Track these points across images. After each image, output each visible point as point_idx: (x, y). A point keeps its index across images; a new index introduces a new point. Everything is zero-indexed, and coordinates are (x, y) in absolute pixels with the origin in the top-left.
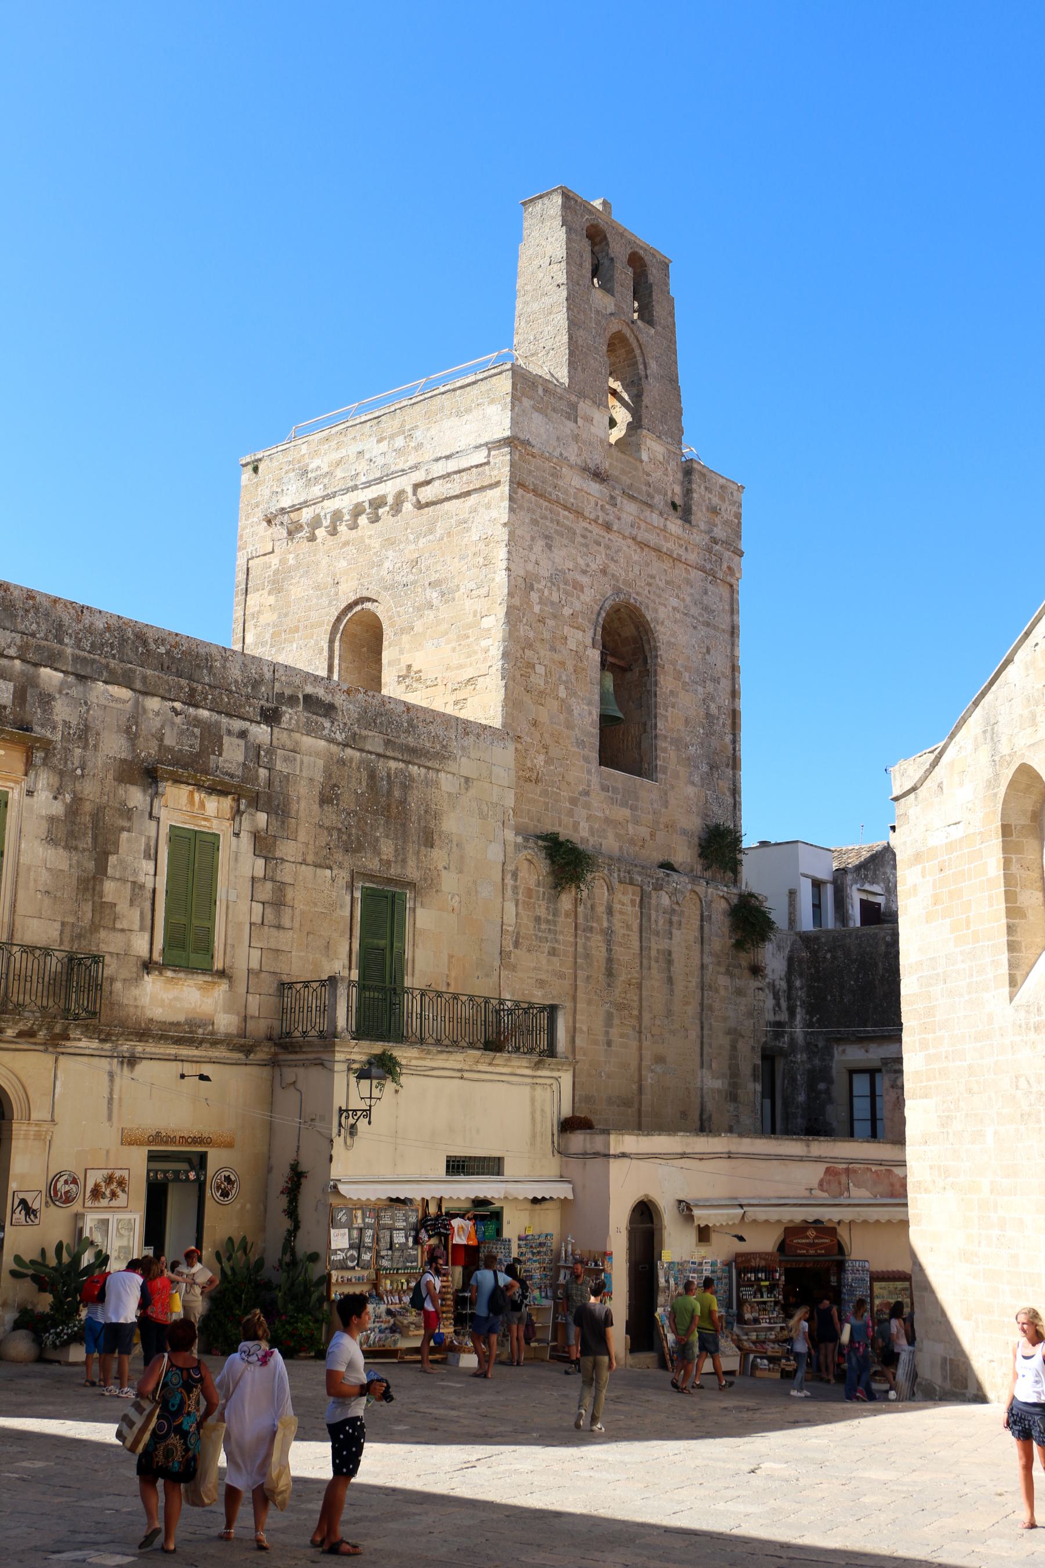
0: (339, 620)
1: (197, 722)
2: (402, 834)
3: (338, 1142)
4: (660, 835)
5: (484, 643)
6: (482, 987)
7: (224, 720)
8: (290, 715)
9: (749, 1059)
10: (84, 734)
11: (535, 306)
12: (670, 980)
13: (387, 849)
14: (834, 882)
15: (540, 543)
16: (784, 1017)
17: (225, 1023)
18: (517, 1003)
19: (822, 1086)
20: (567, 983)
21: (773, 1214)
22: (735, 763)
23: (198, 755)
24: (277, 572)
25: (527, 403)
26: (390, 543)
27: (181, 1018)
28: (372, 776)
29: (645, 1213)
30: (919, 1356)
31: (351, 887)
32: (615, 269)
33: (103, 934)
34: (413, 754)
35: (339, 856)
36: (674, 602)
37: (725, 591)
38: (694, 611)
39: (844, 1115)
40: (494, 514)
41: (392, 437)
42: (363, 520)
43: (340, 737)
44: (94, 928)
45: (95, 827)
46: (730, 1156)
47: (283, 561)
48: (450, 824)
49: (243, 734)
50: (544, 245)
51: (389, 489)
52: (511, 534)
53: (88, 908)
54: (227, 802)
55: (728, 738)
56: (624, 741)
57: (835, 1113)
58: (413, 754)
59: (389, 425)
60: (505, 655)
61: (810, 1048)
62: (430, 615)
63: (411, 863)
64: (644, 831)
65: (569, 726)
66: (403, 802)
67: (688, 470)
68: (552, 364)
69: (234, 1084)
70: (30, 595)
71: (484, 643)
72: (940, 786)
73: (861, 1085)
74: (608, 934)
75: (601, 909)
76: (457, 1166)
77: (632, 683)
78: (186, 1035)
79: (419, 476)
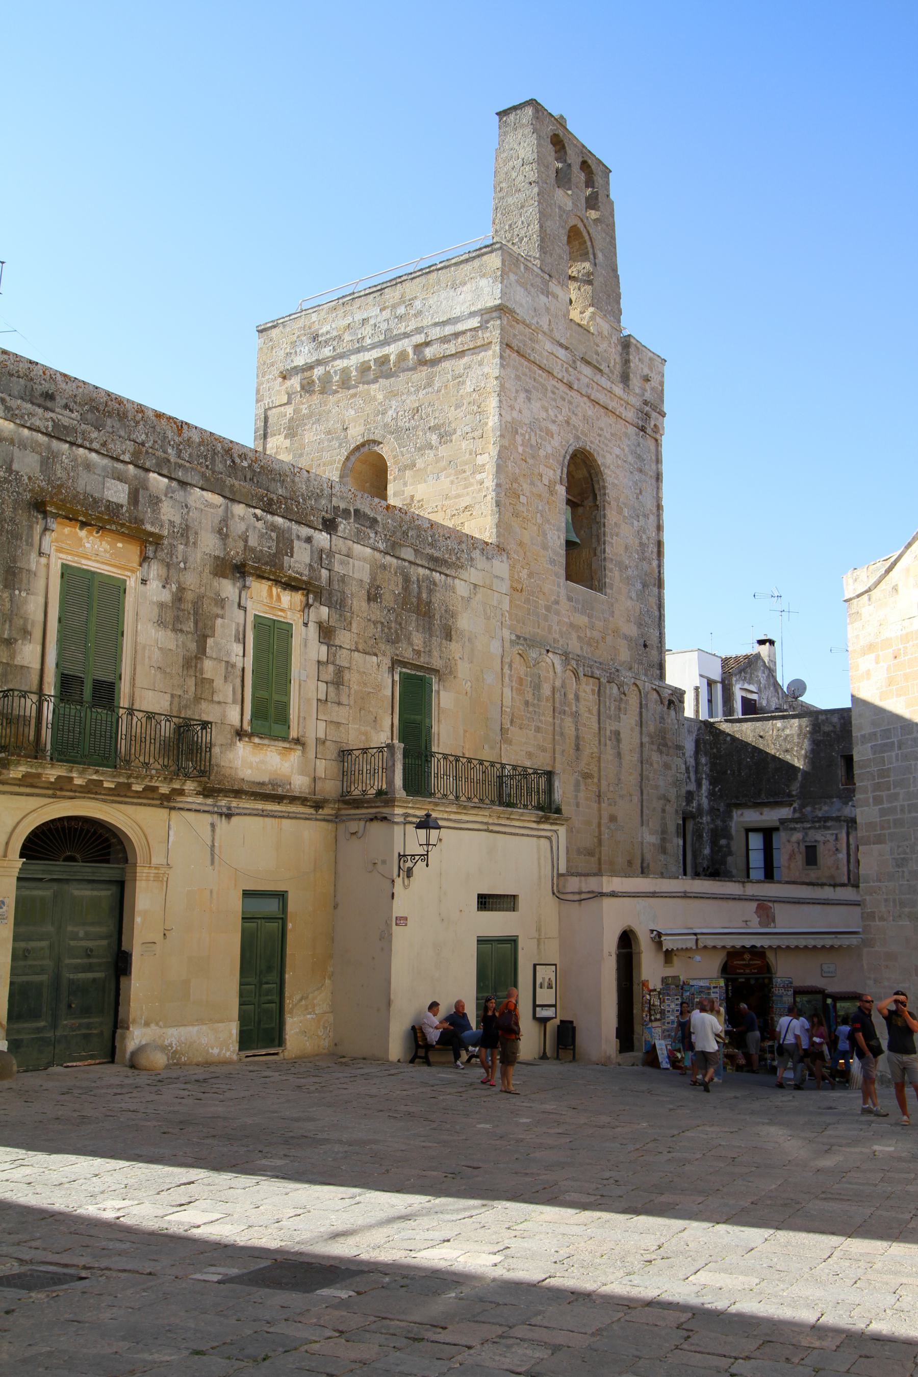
1: (274, 527)
2: (429, 630)
3: (399, 881)
4: (609, 639)
5: (479, 477)
6: (487, 754)
7: (295, 526)
8: (344, 526)
9: (673, 821)
10: (185, 532)
12: (619, 755)
15: (522, 395)
16: (692, 787)
17: (299, 783)
19: (723, 842)
22: (660, 584)
23: (275, 555)
25: (513, 277)
27: (265, 779)
28: (407, 580)
29: (627, 939)
31: (392, 669)
33: (204, 705)
34: (436, 563)
36: (617, 451)
37: (651, 444)
38: (630, 459)
40: (486, 370)
41: (394, 307)
43: (381, 546)
44: (198, 699)
45: (196, 613)
46: (685, 896)
48: (464, 622)
49: (309, 540)
53: (191, 682)
55: (655, 563)
56: (583, 560)
57: (734, 862)
58: (436, 563)
61: (713, 811)
62: (430, 454)
63: (436, 653)
64: (596, 634)
65: (545, 547)
66: (429, 603)
67: (626, 344)
69: (307, 834)
70: (141, 409)
72: (895, 589)
73: (756, 841)
74: (576, 715)
75: (571, 696)
76: (486, 902)
78: (271, 795)
79: (419, 339)
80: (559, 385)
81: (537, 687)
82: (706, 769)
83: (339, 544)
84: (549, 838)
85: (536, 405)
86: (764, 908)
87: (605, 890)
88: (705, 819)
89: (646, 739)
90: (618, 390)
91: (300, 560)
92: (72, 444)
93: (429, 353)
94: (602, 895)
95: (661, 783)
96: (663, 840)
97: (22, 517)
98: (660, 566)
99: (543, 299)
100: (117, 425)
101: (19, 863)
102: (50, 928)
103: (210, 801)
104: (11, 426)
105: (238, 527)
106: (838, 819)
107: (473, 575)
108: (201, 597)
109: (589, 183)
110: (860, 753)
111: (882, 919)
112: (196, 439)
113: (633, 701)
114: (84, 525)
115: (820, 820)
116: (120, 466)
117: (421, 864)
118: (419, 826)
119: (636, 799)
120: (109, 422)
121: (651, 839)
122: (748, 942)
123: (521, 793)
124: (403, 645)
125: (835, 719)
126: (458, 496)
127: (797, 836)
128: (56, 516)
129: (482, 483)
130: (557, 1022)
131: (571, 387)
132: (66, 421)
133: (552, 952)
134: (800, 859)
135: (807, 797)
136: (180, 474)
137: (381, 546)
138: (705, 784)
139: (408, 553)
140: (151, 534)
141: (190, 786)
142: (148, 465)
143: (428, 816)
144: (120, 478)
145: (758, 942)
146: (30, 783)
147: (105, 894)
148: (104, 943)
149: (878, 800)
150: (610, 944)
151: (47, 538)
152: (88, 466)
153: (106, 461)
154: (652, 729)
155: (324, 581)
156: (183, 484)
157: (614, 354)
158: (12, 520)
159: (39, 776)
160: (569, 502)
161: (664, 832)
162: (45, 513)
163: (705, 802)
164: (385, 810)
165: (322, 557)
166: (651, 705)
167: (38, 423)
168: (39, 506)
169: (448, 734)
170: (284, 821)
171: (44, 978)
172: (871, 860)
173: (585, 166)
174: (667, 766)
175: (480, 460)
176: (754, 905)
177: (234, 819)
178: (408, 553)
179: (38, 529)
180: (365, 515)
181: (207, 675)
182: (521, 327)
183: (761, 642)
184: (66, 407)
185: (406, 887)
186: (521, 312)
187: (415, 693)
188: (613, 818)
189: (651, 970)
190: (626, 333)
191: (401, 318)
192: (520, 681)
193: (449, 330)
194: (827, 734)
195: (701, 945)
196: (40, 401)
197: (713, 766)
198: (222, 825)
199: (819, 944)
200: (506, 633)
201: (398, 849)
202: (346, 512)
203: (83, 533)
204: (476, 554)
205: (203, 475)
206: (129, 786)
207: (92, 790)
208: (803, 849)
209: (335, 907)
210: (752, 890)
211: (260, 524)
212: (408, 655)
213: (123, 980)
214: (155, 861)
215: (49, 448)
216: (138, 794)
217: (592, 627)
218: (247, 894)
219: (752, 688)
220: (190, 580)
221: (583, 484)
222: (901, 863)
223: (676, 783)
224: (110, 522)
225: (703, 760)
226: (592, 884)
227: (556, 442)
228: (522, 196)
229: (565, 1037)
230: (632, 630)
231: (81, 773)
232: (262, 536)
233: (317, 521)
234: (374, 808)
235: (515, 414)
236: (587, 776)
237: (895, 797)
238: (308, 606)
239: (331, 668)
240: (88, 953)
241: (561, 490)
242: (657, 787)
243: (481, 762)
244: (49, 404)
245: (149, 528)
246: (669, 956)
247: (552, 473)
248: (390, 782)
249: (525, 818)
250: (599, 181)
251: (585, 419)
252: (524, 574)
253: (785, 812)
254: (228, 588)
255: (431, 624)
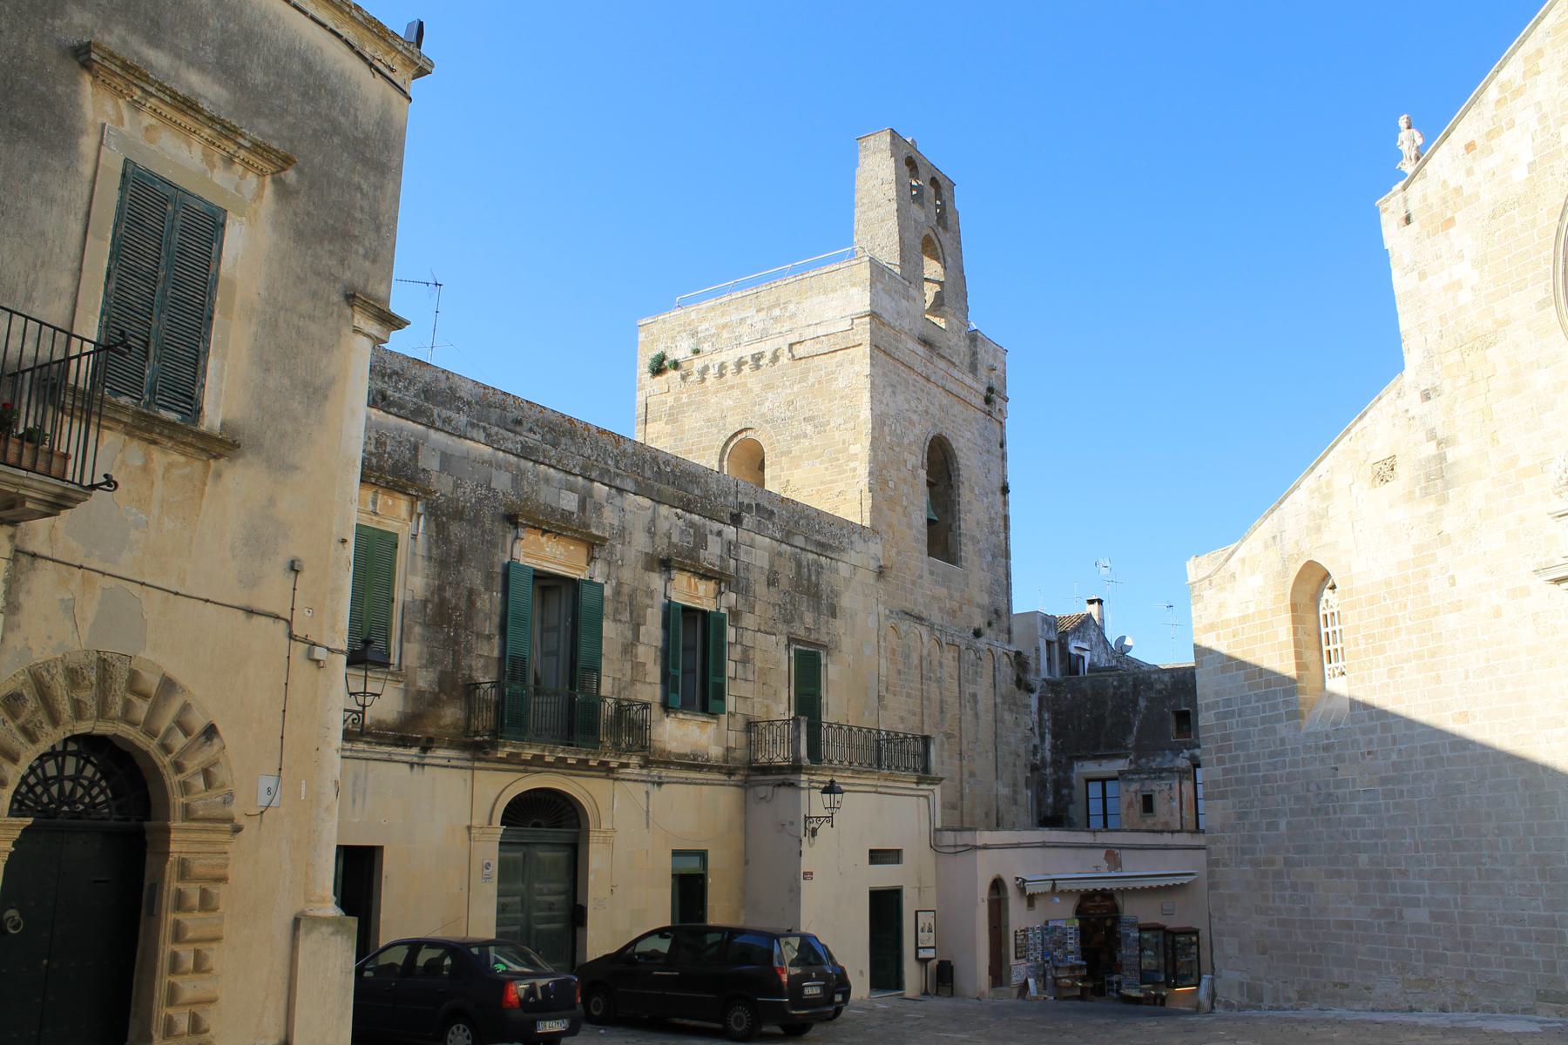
0: (726, 444)
1: (692, 524)
2: (817, 609)
3: (805, 840)
4: (965, 608)
5: (852, 465)
6: (868, 722)
7: (708, 522)
8: (748, 520)
9: (1023, 774)
10: (622, 533)
11: (871, 214)
12: (976, 716)
13: (809, 618)
14: (1059, 640)
15: (889, 390)
16: (1037, 741)
17: (715, 752)
18: (888, 733)
19: (1065, 791)
20: (917, 718)
21: (1075, 886)
22: (1007, 556)
23: (692, 549)
24: (672, 408)
25: (879, 286)
26: (769, 387)
27: (687, 750)
28: (799, 565)
29: (997, 885)
30: (1218, 982)
31: (788, 646)
32: (927, 193)
33: (638, 686)
34: (823, 548)
35: (780, 626)
36: (968, 435)
37: (997, 426)
38: (980, 441)
39: (1082, 808)
40: (857, 368)
41: (770, 308)
42: (746, 369)
43: (778, 535)
44: (633, 681)
45: (631, 604)
46: (1044, 845)
47: (677, 400)
48: (846, 601)
49: (719, 533)
50: (877, 173)
51: (767, 347)
52: (872, 383)
53: (628, 666)
54: (712, 585)
55: (1002, 536)
56: (942, 538)
57: (1076, 812)
58: (823, 548)
59: (766, 298)
60: (871, 473)
61: (1055, 763)
62: (806, 442)
63: (823, 630)
64: (955, 605)
65: (910, 527)
66: (817, 585)
67: (973, 337)
68: (890, 256)
69: (721, 798)
70: (587, 426)
71: (852, 465)
72: (1233, 576)
73: (1095, 789)
74: (939, 680)
75: (935, 663)
76: (877, 856)
77: (946, 492)
78: (693, 763)
79: (793, 338)
80: (919, 379)
81: (908, 657)
82: (1048, 724)
83: (744, 536)
84: (926, 797)
85: (900, 398)
86: (1112, 854)
87: (979, 843)
88: (1049, 771)
89: (999, 700)
90: (969, 379)
91: (712, 553)
92: (536, 462)
93: (799, 351)
94: (977, 848)
95: (1012, 740)
96: (1015, 792)
97: (498, 527)
98: (1007, 538)
99: (904, 302)
100: (569, 442)
101: (501, 830)
102: (520, 886)
103: (645, 772)
104: (490, 450)
105: (663, 526)
106: (1170, 770)
107: (852, 557)
108: (635, 590)
109: (938, 195)
110: (1205, 719)
111: (1225, 865)
112: (630, 450)
113: (987, 664)
114: (545, 532)
115: (1155, 771)
116: (571, 478)
117: (826, 825)
118: (825, 791)
119: (991, 755)
120: (563, 440)
121: (1004, 791)
122: (1099, 886)
123: (899, 756)
124: (796, 624)
125: (1166, 678)
126: (833, 482)
127: (1135, 787)
128: (526, 526)
129: (854, 470)
130: (935, 962)
131: (928, 380)
132: (531, 443)
133: (931, 901)
134: (1138, 807)
135: (1142, 750)
136: (618, 482)
137: (778, 535)
138: (1048, 737)
139: (799, 541)
140: (598, 537)
141: (635, 760)
142: (593, 475)
143: (832, 782)
144: (572, 489)
145: (1107, 885)
146: (514, 761)
147: (561, 855)
148: (563, 897)
149: (1221, 761)
150: (983, 891)
151: (518, 545)
152: (547, 480)
153: (561, 475)
154: (1004, 690)
155: (732, 569)
156: (620, 490)
157: (963, 346)
158: (491, 531)
159: (519, 755)
160: (930, 484)
161: (1015, 785)
162: (516, 525)
163: (1048, 755)
164: (792, 778)
165: (731, 548)
166: (1003, 668)
167: (510, 446)
168: (512, 520)
169: (836, 706)
170: (704, 788)
171: (516, 928)
172: (1213, 814)
173: (934, 182)
174: (1017, 724)
175: (853, 449)
176: (1103, 852)
177: (664, 787)
178: (799, 541)
179: (510, 538)
180: (765, 509)
181: (641, 659)
182: (886, 329)
183: (1091, 602)
184: (531, 430)
185: (811, 845)
186: (886, 317)
187: (808, 668)
188: (972, 774)
189: (1019, 917)
190: (974, 326)
191: (776, 320)
192: (894, 651)
193: (821, 331)
194: (1160, 692)
195: (1058, 889)
196: (511, 426)
197: (1055, 722)
198: (654, 790)
199: (1155, 884)
200: (881, 608)
201: (804, 811)
202: (749, 506)
203: (544, 539)
204: (855, 537)
205: (637, 482)
206: (587, 761)
207: (560, 764)
208: (1140, 798)
209: (746, 863)
210: (1103, 838)
211: (680, 523)
212: (802, 633)
213: (579, 930)
214: (604, 826)
215: (518, 467)
216: (571, 766)
217: (951, 598)
218: (676, 853)
219: (1085, 646)
220: (626, 575)
221: (941, 463)
222: (1242, 816)
223: (1027, 739)
224: (566, 529)
225: (1046, 716)
226: (966, 838)
227: (917, 431)
228: (881, 211)
229: (943, 977)
230: (984, 599)
231: (551, 752)
232: (682, 532)
233: (727, 519)
234: (785, 775)
235: (883, 407)
236: (949, 736)
237: (1236, 758)
238: (720, 593)
239: (739, 647)
240: (550, 906)
241: (923, 474)
242: (1008, 744)
243: (860, 729)
244: (518, 429)
245: (594, 531)
246: (1031, 900)
247: (915, 459)
248: (796, 751)
249: (908, 782)
250: (945, 194)
251: (941, 408)
252: (893, 552)
253: (1121, 765)
254: (656, 581)
255: (819, 603)
